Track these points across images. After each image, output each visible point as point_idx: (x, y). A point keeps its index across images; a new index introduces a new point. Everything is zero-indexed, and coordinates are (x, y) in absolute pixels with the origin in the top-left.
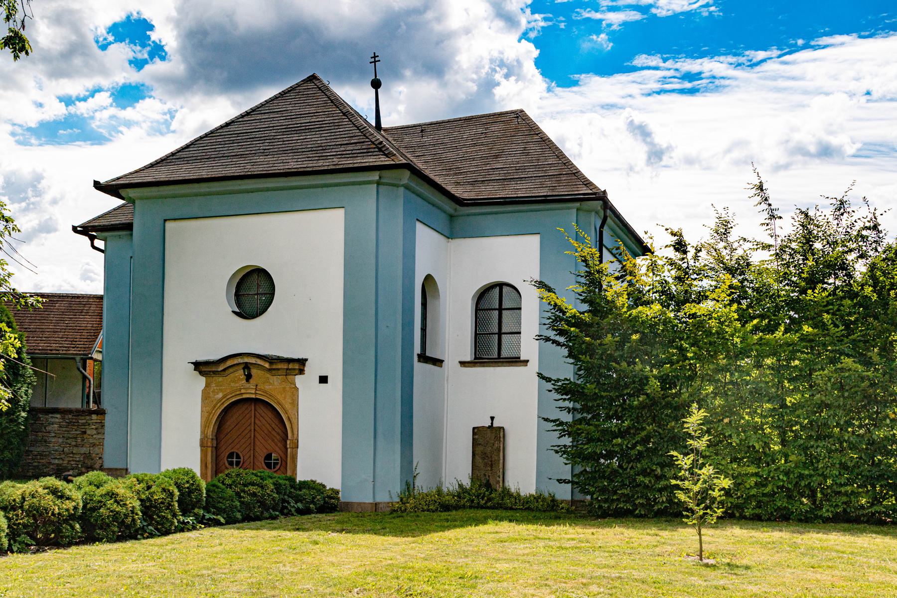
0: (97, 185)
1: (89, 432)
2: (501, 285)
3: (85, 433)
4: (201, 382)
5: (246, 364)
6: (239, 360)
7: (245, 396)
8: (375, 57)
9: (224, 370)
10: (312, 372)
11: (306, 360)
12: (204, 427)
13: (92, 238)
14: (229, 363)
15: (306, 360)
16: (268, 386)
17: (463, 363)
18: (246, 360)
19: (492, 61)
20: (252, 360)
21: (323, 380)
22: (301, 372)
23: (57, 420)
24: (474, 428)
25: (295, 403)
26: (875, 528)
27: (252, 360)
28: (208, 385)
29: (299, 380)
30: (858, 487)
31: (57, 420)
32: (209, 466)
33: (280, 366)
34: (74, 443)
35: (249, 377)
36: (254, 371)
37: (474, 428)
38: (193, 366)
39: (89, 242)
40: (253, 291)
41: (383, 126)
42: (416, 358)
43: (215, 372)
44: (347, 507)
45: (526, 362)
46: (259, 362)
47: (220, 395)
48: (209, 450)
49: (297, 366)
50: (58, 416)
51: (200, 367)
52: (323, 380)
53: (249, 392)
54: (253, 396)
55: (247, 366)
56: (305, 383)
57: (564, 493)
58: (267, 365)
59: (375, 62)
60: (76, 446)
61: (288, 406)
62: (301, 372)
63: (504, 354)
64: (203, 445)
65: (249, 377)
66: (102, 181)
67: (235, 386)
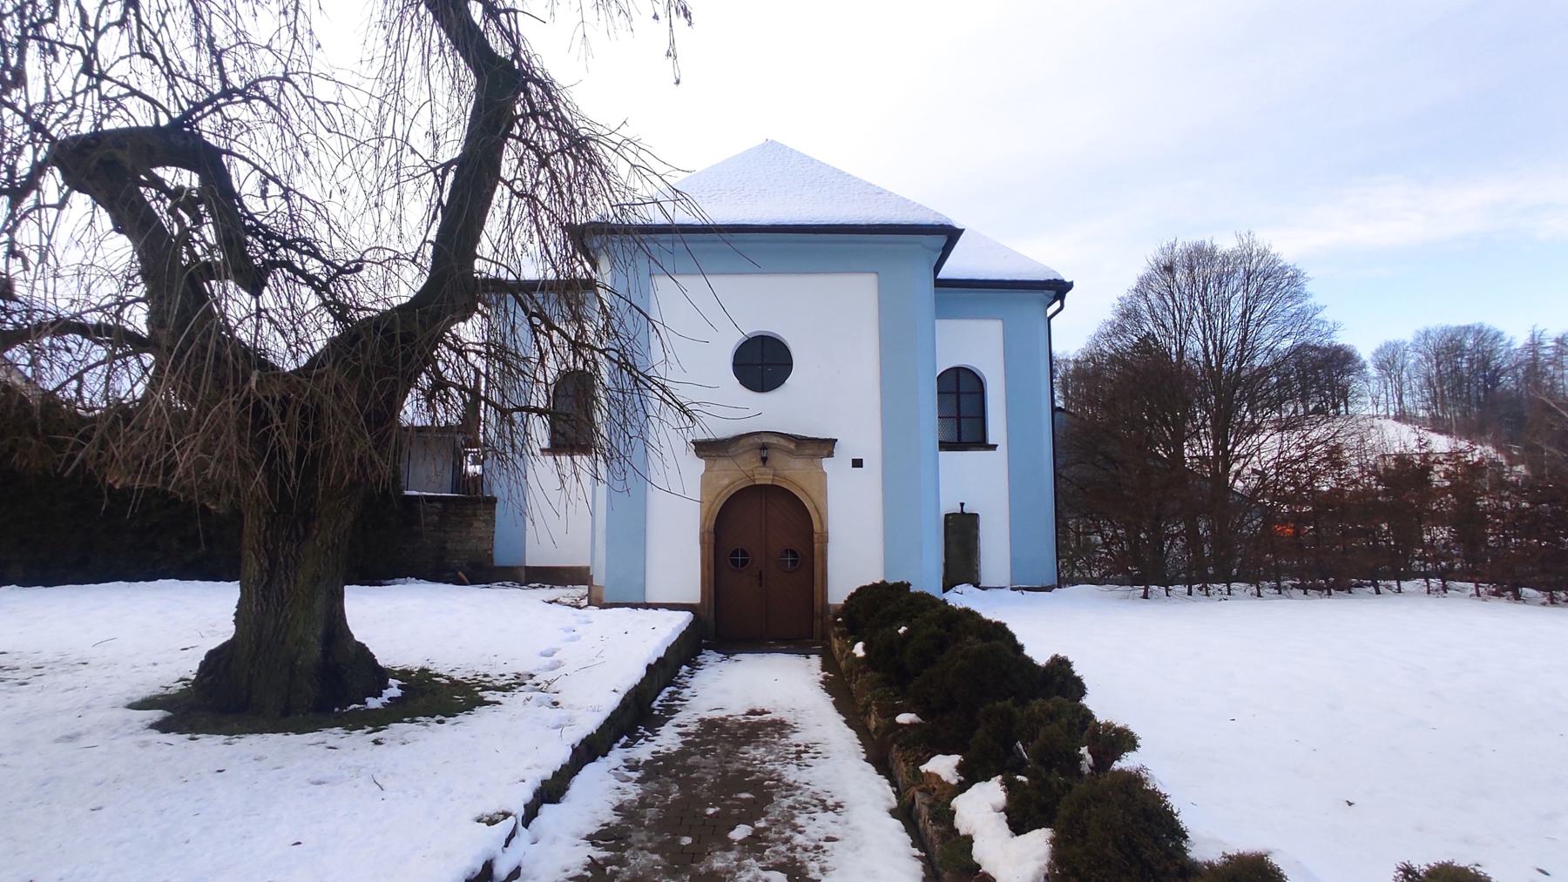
4: (700, 465)
5: (763, 445)
6: (757, 440)
10: (843, 455)
12: (702, 526)
16: (793, 472)
18: (765, 440)
19: (814, 795)
20: (774, 440)
21: (857, 463)
22: (830, 455)
25: (823, 491)
27: (774, 440)
29: (827, 464)
35: (764, 460)
37: (974, 518)
40: (763, 362)
44: (916, 824)
45: (994, 447)
46: (782, 442)
47: (726, 482)
52: (857, 463)
53: (764, 477)
55: (764, 447)
58: (792, 446)
61: (814, 494)
62: (830, 455)
63: (964, 439)
64: (702, 542)
65: (764, 460)
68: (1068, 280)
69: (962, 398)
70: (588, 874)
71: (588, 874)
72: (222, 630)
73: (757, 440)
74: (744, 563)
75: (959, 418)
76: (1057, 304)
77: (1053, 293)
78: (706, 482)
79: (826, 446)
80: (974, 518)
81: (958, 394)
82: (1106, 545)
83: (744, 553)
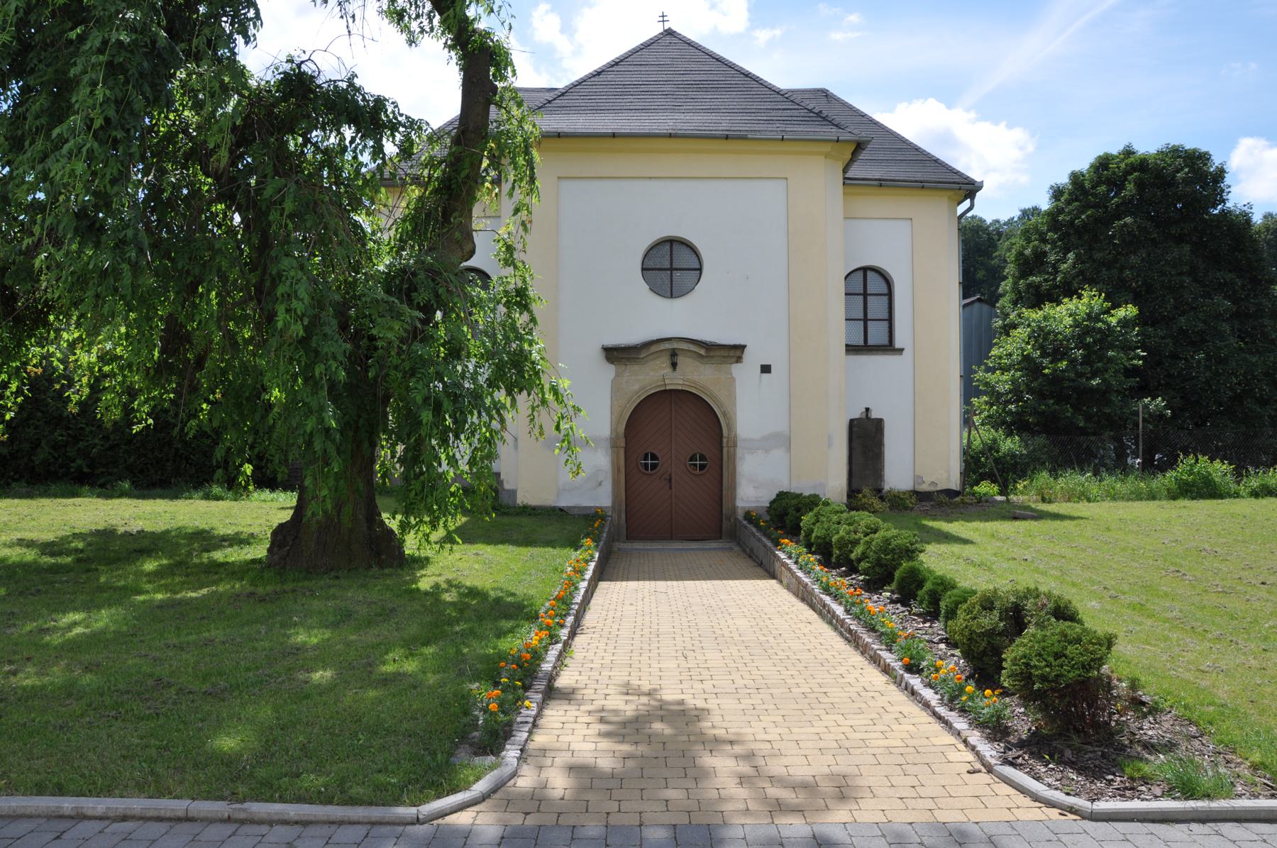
2: (700, 269)
4: (609, 371)
5: (672, 350)
6: (667, 346)
10: (753, 359)
11: (744, 347)
14: (654, 348)
15: (744, 347)
16: (693, 375)
18: (676, 345)
21: (766, 369)
26: (159, 491)
27: (685, 346)
28: (617, 375)
29: (736, 369)
30: (177, 449)
33: (718, 353)
35: (674, 365)
37: (880, 422)
40: (671, 264)
45: (901, 351)
46: (692, 348)
51: (614, 354)
52: (766, 369)
56: (745, 373)
57: (1010, 444)
58: (702, 352)
62: (739, 359)
63: (870, 342)
65: (674, 365)
67: (653, 376)
68: (978, 180)
69: (861, 316)
70: (1024, 179)
71: (1024, 179)
72: (286, 516)
73: (667, 346)
74: (654, 467)
75: (865, 320)
76: (967, 203)
77: (963, 193)
78: (616, 389)
79: (735, 352)
80: (880, 422)
81: (865, 295)
82: (58, 244)
83: (654, 457)
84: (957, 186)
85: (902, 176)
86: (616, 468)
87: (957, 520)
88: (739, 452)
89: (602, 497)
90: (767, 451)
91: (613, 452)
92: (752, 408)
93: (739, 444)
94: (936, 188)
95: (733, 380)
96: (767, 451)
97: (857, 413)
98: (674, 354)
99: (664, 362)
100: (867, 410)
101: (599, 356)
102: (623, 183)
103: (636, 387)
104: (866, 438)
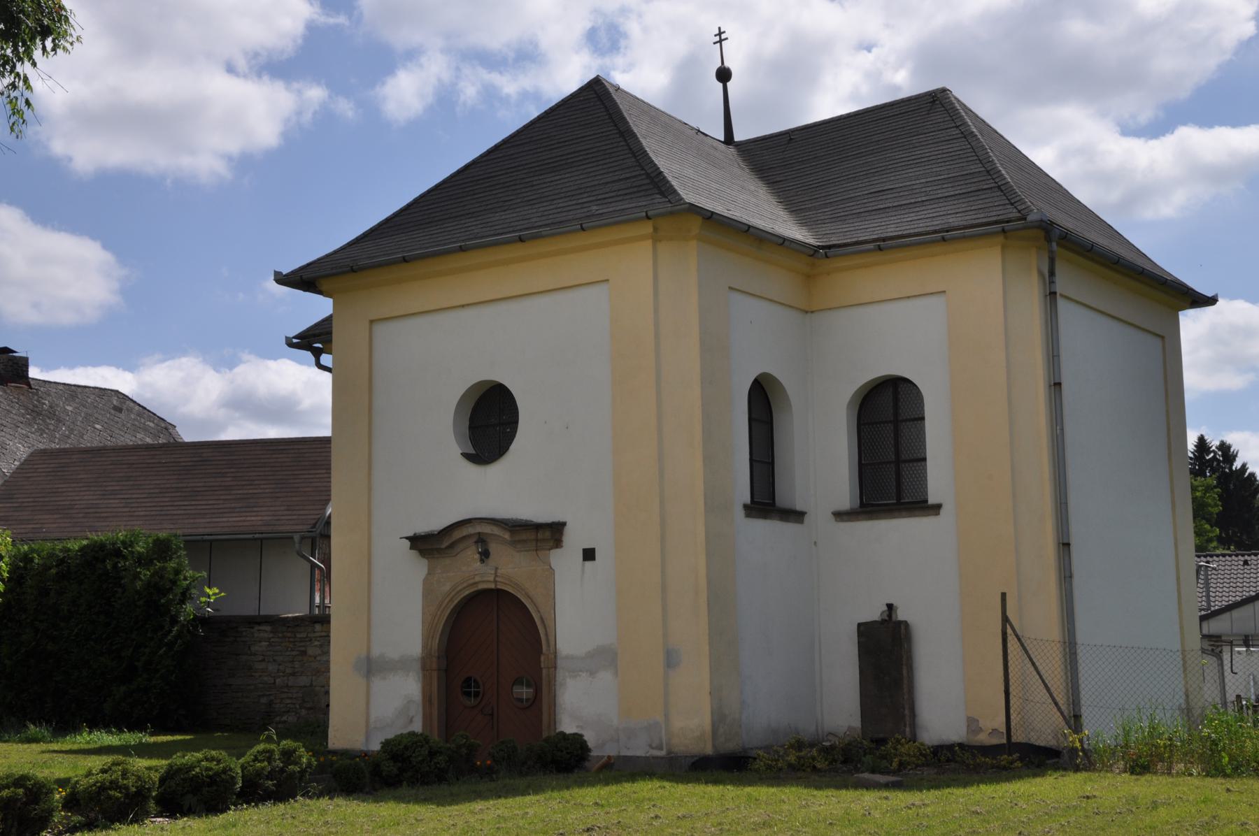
0: (282, 279)
1: (310, 651)
3: (304, 653)
7: (481, 586)
8: (720, 33)
9: (448, 547)
10: (575, 540)
11: (564, 524)
13: (317, 354)
14: (457, 534)
15: (564, 524)
16: (510, 568)
17: (840, 515)
18: (487, 529)
23: (266, 635)
24: (859, 625)
27: (487, 529)
31: (266, 635)
32: (435, 702)
34: (289, 671)
35: (485, 555)
36: (493, 547)
37: (859, 625)
38: (408, 543)
39: (313, 359)
40: (490, 421)
41: (736, 139)
42: (740, 512)
43: (439, 551)
45: (937, 508)
48: (435, 674)
49: (548, 534)
50: (268, 628)
51: (423, 544)
54: (493, 586)
55: (481, 540)
56: (565, 561)
59: (721, 41)
60: (293, 674)
62: (558, 543)
65: (485, 555)
66: (286, 270)
67: (468, 571)
78: (428, 590)
79: (553, 533)
84: (871, 246)
85: (922, 226)
86: (427, 699)
87: (792, 785)
88: (560, 675)
89: (1014, 739)
90: (592, 673)
91: (424, 676)
92: (577, 610)
93: (559, 662)
94: (964, 237)
95: (551, 571)
96: (592, 673)
97: (873, 613)
98: (481, 540)
99: (471, 554)
100: (890, 607)
101: (832, 518)
102: (503, 307)
103: (447, 587)
104: (885, 649)
